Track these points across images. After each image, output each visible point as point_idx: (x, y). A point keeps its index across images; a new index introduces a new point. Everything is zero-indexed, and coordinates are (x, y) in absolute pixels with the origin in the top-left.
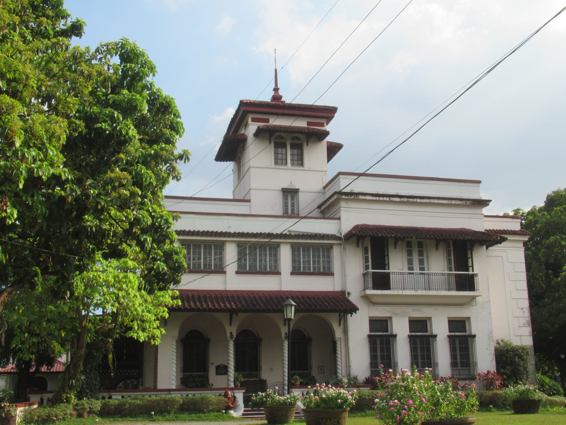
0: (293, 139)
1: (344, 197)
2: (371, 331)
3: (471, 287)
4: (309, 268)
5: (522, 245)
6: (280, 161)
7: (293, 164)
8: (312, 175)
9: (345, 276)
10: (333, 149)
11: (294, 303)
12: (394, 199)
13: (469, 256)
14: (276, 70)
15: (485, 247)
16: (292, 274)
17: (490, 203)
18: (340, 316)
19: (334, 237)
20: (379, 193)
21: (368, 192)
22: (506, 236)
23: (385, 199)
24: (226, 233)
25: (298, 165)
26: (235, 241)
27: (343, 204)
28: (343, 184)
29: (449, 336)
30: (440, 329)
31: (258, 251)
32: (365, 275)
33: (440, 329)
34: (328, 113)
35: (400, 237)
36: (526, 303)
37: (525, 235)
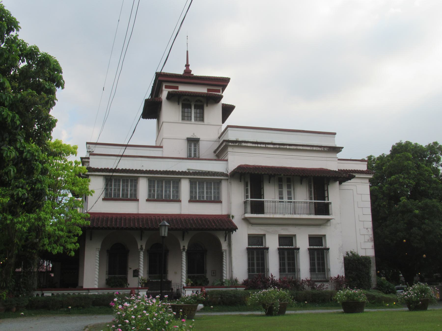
0: (197, 101)
1: (230, 144)
2: (280, 245)
3: (327, 213)
4: (203, 197)
5: (367, 181)
6: (185, 117)
7: (196, 120)
8: (209, 129)
9: (231, 203)
10: (227, 110)
11: (167, 224)
12: (269, 146)
13: (326, 189)
14: (187, 52)
15: (338, 182)
16: (190, 201)
17: (343, 150)
18: (226, 233)
19: (222, 174)
20: (258, 141)
21: (249, 141)
22: (354, 174)
23: (262, 146)
24: (140, 170)
25: (200, 120)
26: (147, 177)
27: (230, 149)
28: (232, 135)
29: (247, 248)
30: (302, 243)
31: (164, 184)
32: (245, 203)
33: (302, 243)
34: (223, 83)
35: (271, 174)
36: (370, 225)
37: (370, 174)
